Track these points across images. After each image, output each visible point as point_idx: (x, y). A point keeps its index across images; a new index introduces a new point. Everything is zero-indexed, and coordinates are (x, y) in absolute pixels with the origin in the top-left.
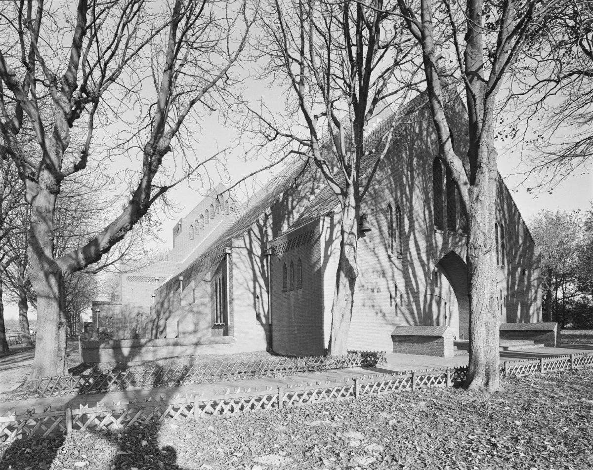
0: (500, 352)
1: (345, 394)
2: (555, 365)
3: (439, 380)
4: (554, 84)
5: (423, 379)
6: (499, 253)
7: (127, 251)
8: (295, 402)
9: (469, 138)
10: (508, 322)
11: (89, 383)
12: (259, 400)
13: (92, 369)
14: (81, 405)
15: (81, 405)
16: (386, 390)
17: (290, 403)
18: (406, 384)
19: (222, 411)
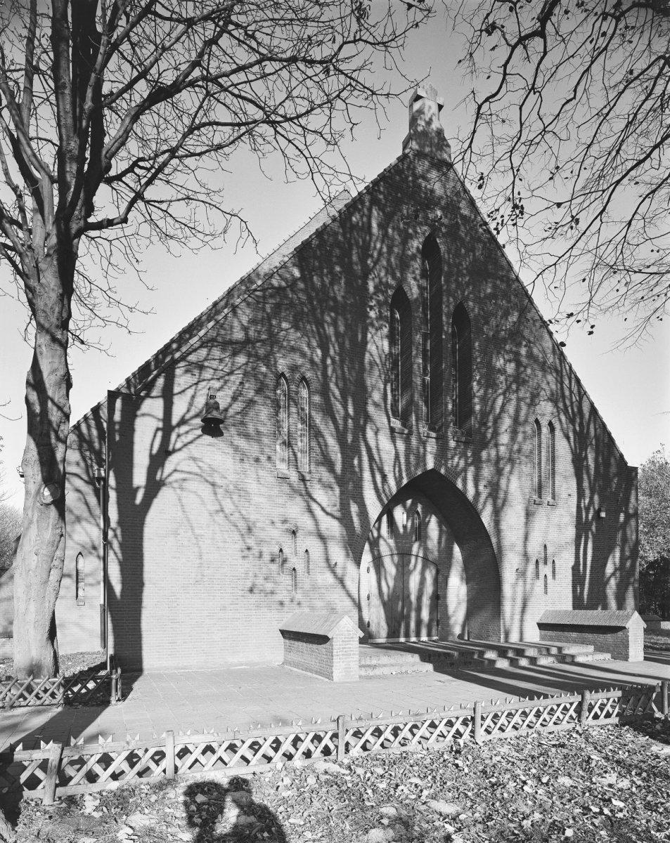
0: (48, 759)
1: (462, 730)
2: (602, 709)
3: (596, 713)
4: (537, 43)
5: (568, 710)
6: (543, 454)
7: (241, 77)
8: (386, 742)
9: (360, 268)
10: (574, 608)
11: (87, 688)
12: (357, 734)
13: (351, 502)
14: (42, 742)
15: (42, 742)
16: (564, 722)
17: (378, 746)
18: (534, 721)
19: (308, 754)
